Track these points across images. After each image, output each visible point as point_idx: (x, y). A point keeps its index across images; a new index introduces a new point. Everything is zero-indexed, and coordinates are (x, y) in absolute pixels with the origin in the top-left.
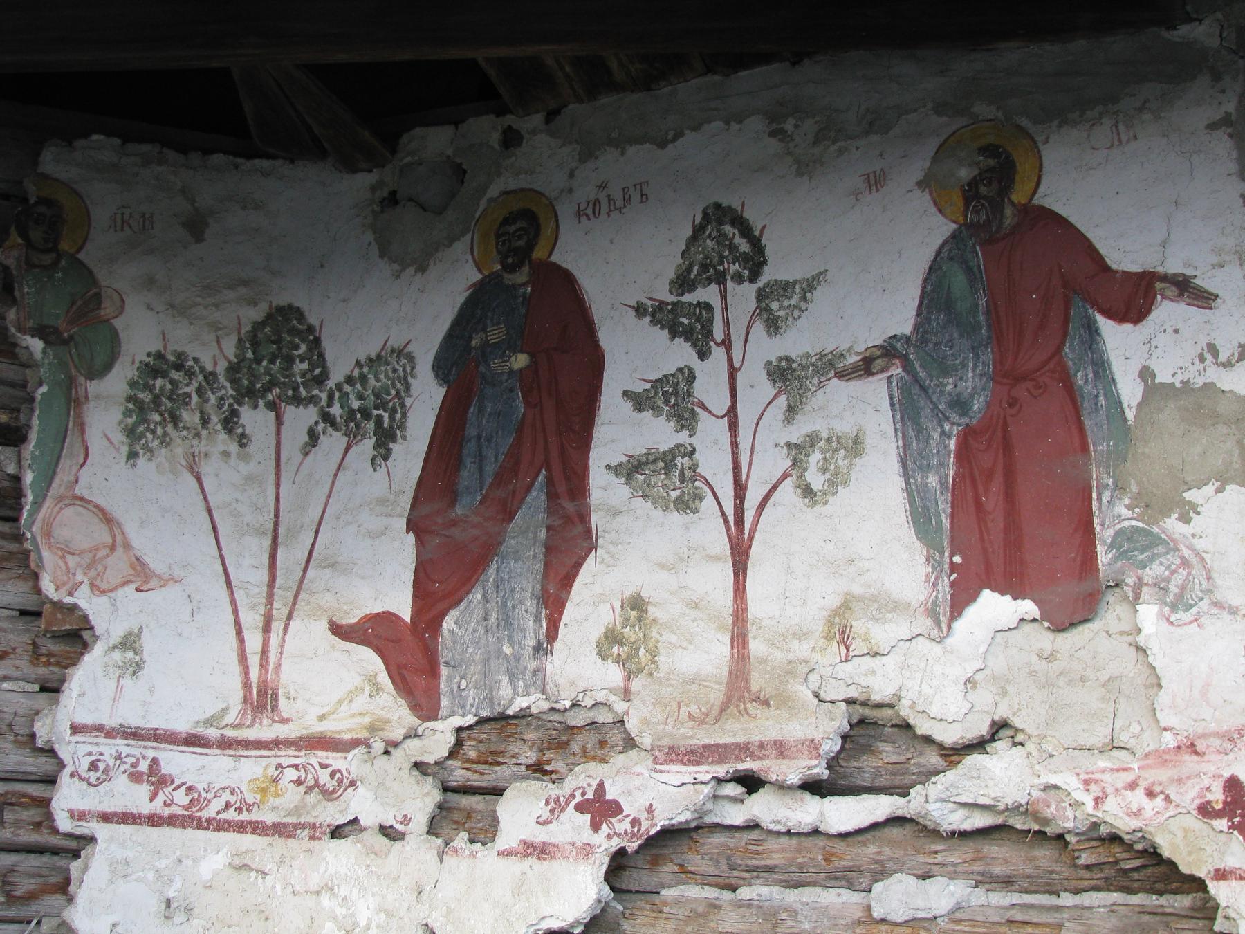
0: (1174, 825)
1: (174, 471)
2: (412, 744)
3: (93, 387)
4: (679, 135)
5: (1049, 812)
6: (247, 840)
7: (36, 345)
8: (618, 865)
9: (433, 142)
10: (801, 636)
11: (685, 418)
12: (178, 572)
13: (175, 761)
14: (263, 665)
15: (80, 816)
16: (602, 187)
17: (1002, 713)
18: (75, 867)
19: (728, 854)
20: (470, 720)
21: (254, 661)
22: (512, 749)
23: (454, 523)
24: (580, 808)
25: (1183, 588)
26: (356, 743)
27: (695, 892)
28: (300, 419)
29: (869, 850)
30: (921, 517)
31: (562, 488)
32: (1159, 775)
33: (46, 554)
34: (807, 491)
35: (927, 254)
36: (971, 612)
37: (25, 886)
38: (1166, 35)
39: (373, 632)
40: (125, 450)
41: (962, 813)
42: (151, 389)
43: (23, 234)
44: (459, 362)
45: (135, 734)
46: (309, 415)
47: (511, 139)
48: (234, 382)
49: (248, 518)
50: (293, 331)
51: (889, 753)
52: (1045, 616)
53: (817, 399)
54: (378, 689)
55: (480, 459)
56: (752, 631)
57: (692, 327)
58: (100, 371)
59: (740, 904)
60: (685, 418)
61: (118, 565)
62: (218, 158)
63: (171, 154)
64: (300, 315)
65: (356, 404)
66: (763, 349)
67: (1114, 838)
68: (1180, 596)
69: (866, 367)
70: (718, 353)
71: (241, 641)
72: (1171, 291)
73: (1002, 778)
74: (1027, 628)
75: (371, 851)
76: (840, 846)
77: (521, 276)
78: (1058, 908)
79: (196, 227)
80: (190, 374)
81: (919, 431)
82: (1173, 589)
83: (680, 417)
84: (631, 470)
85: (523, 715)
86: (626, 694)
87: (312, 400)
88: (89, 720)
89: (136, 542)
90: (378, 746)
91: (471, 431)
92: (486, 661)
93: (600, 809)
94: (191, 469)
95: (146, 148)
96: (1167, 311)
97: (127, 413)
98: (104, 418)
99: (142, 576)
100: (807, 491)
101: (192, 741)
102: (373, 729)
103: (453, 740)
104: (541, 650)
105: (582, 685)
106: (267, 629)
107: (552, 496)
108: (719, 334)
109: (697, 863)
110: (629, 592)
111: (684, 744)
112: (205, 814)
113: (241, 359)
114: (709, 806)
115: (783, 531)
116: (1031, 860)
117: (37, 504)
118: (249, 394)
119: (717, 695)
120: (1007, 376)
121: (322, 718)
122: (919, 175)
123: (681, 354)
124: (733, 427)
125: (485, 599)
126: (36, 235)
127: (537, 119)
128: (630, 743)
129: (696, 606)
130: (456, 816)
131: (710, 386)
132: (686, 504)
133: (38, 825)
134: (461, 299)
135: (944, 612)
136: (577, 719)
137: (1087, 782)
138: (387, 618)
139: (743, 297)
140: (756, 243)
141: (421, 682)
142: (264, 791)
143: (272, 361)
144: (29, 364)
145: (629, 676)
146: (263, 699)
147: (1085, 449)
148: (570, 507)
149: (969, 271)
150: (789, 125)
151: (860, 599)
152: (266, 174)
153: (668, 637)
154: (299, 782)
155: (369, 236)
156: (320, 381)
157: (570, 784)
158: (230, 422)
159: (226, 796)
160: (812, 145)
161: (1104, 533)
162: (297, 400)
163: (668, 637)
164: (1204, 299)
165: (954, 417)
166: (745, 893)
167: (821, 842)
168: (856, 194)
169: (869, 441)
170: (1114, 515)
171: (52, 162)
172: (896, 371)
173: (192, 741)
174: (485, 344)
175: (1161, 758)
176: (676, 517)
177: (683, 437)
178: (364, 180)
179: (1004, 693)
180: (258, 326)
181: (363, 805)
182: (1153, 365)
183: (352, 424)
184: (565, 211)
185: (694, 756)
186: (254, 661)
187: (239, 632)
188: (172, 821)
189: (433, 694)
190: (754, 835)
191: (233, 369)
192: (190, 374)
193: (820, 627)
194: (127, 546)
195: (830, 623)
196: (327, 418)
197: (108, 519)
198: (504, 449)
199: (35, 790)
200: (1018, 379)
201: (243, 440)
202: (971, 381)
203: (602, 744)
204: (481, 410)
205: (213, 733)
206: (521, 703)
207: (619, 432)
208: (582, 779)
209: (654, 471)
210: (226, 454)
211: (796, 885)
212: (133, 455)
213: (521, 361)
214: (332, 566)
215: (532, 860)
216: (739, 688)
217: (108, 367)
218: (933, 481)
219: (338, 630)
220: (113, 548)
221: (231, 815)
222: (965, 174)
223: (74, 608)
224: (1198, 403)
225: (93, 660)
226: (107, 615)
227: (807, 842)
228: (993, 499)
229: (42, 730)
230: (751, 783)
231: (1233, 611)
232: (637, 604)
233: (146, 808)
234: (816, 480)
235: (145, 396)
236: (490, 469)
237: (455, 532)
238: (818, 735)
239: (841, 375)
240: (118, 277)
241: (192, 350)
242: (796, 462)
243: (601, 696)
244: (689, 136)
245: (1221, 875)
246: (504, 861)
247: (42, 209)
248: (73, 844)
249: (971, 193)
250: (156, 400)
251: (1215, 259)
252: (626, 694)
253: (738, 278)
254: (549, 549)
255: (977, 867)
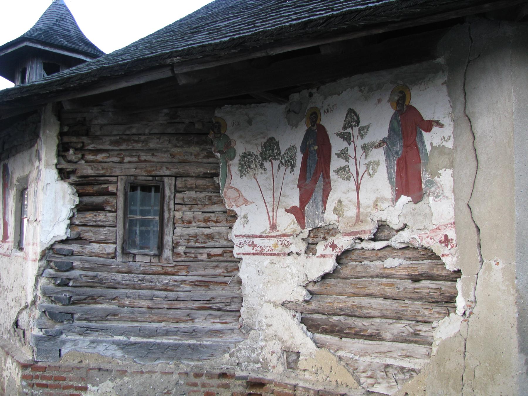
0: (435, 245)
1: (251, 179)
2: (301, 234)
3: (231, 162)
4: (342, 92)
5: (413, 243)
6: (273, 257)
7: (219, 155)
8: (338, 259)
9: (295, 97)
10: (369, 207)
11: (347, 160)
12: (254, 200)
13: (257, 241)
14: (273, 219)
15: (239, 254)
16: (329, 105)
17: (405, 222)
18: (239, 265)
19: (359, 255)
20: (311, 229)
21: (271, 218)
22: (319, 234)
23: (306, 185)
24: (330, 247)
25: (438, 193)
26: (291, 235)
27: (354, 263)
28: (276, 163)
29: (383, 253)
30: (390, 179)
31: (325, 176)
32: (433, 235)
33: (226, 200)
34: (370, 174)
35: (390, 118)
36: (400, 200)
37: (230, 269)
38: (434, 61)
39: (292, 210)
40: (240, 175)
41: (399, 244)
42: (244, 161)
43: (213, 131)
44: (305, 148)
45: (248, 236)
46: (278, 162)
47: (311, 95)
48: (262, 157)
49: (267, 187)
50: (273, 143)
51: (386, 232)
52: (413, 201)
53: (371, 153)
54: (294, 223)
55: (310, 170)
56: (361, 206)
57: (346, 137)
58: (232, 158)
59: (361, 265)
60: (347, 160)
61: (241, 200)
62: (253, 105)
63: (242, 106)
64: (274, 139)
65: (287, 159)
66: (360, 142)
67: (426, 249)
68: (437, 195)
69: (379, 146)
70: (352, 143)
71: (269, 214)
72: (435, 124)
73: (405, 236)
74: (410, 203)
75: (295, 258)
76: (378, 252)
77: (315, 128)
78: (419, 264)
79: (250, 122)
80: (252, 156)
81: (390, 159)
82: (436, 193)
83: (346, 159)
84: (337, 171)
85: (321, 227)
86: (338, 221)
87: (278, 159)
88: (238, 234)
89: (244, 195)
90: (295, 235)
91: (308, 164)
92: (313, 216)
93: (334, 246)
94: (254, 177)
95: (237, 106)
96: (435, 129)
97: (239, 167)
98: (234, 169)
99: (246, 202)
100: (370, 174)
101: (260, 237)
102: (294, 232)
103: (308, 233)
104: (323, 213)
105: (330, 220)
106: (273, 211)
107: (324, 178)
108: (352, 139)
109: (354, 257)
110: (338, 199)
111: (348, 232)
112: (264, 252)
113: (263, 151)
114: (354, 245)
115: (366, 183)
116: (413, 254)
117: (223, 189)
118: (265, 159)
119: (354, 221)
120: (406, 146)
121: (285, 230)
122: (388, 99)
123: (345, 144)
124: (356, 160)
125: (313, 202)
126: (216, 130)
127: (315, 90)
128: (340, 232)
129: (350, 201)
130: (311, 249)
131: (351, 152)
132: (348, 179)
133: (231, 256)
134: (304, 134)
135: (394, 200)
136: (331, 227)
137: (419, 237)
138: (295, 207)
139: (356, 130)
140: (358, 117)
141: (302, 221)
142: (275, 246)
143: (269, 151)
144: (218, 159)
145: (339, 217)
146: (273, 227)
147: (420, 162)
148: (327, 180)
149: (398, 122)
150: (363, 88)
151: (379, 198)
152: (264, 107)
153: (346, 209)
154: (281, 244)
155: (286, 120)
156: (279, 154)
157: (328, 241)
158: (262, 166)
159: (268, 248)
160: (368, 93)
161: (424, 181)
162: (275, 159)
163: (346, 209)
164: (441, 126)
165: (396, 156)
166: (363, 263)
167: (375, 251)
168: (376, 104)
169: (381, 162)
170: (426, 177)
171: (218, 113)
172: (385, 146)
173: (260, 237)
174: (309, 144)
175: (433, 231)
176: (346, 182)
177: (346, 163)
178: (284, 106)
179: (406, 218)
180: (266, 143)
181: (293, 248)
182: (433, 142)
183: (286, 164)
184: (322, 112)
185: (349, 234)
186: (271, 218)
187: (268, 212)
188: (257, 254)
189: (304, 223)
190: (363, 251)
191: (261, 154)
192: (252, 156)
193: (372, 205)
194: (242, 196)
195: (374, 204)
196: (281, 162)
197: (238, 191)
198: (314, 168)
199: (230, 249)
200: (408, 147)
201: (265, 170)
202: (398, 148)
203: (336, 232)
204: (310, 159)
205: (264, 235)
206: (320, 224)
207: (336, 163)
208: (330, 240)
209: (343, 171)
210: (262, 173)
211: (372, 261)
212: (241, 176)
213: (316, 147)
214: (284, 196)
215: (322, 258)
216: (358, 219)
217: (234, 157)
218: (392, 171)
219: (287, 211)
220: (239, 197)
221: (269, 252)
222: (396, 98)
223: (233, 211)
224: (440, 150)
225: (238, 221)
226: (240, 211)
227: (373, 252)
228: (403, 175)
229: (229, 236)
230: (362, 240)
231: (447, 198)
232: (340, 201)
233: (252, 252)
234: (371, 172)
235: (243, 163)
236: (312, 173)
237: (306, 187)
238: (371, 229)
239: (375, 147)
240: (234, 137)
241: (252, 151)
242: (367, 168)
243: (334, 222)
244: (344, 93)
245: (443, 255)
246: (318, 259)
247: (216, 124)
248: (239, 260)
249: (398, 103)
250: (245, 163)
251: (443, 116)
252: (338, 221)
253: (355, 126)
254: (324, 190)
255: (403, 256)
